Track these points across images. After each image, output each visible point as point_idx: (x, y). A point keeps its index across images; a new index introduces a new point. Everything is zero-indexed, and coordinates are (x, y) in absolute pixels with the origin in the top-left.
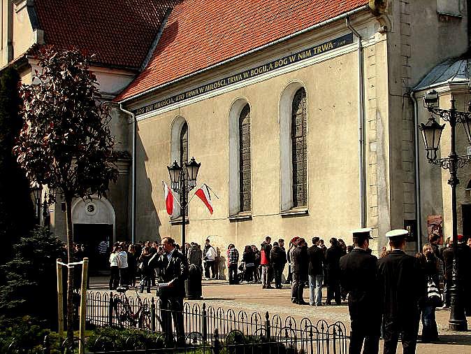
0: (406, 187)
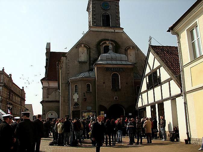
0: (66, 107)
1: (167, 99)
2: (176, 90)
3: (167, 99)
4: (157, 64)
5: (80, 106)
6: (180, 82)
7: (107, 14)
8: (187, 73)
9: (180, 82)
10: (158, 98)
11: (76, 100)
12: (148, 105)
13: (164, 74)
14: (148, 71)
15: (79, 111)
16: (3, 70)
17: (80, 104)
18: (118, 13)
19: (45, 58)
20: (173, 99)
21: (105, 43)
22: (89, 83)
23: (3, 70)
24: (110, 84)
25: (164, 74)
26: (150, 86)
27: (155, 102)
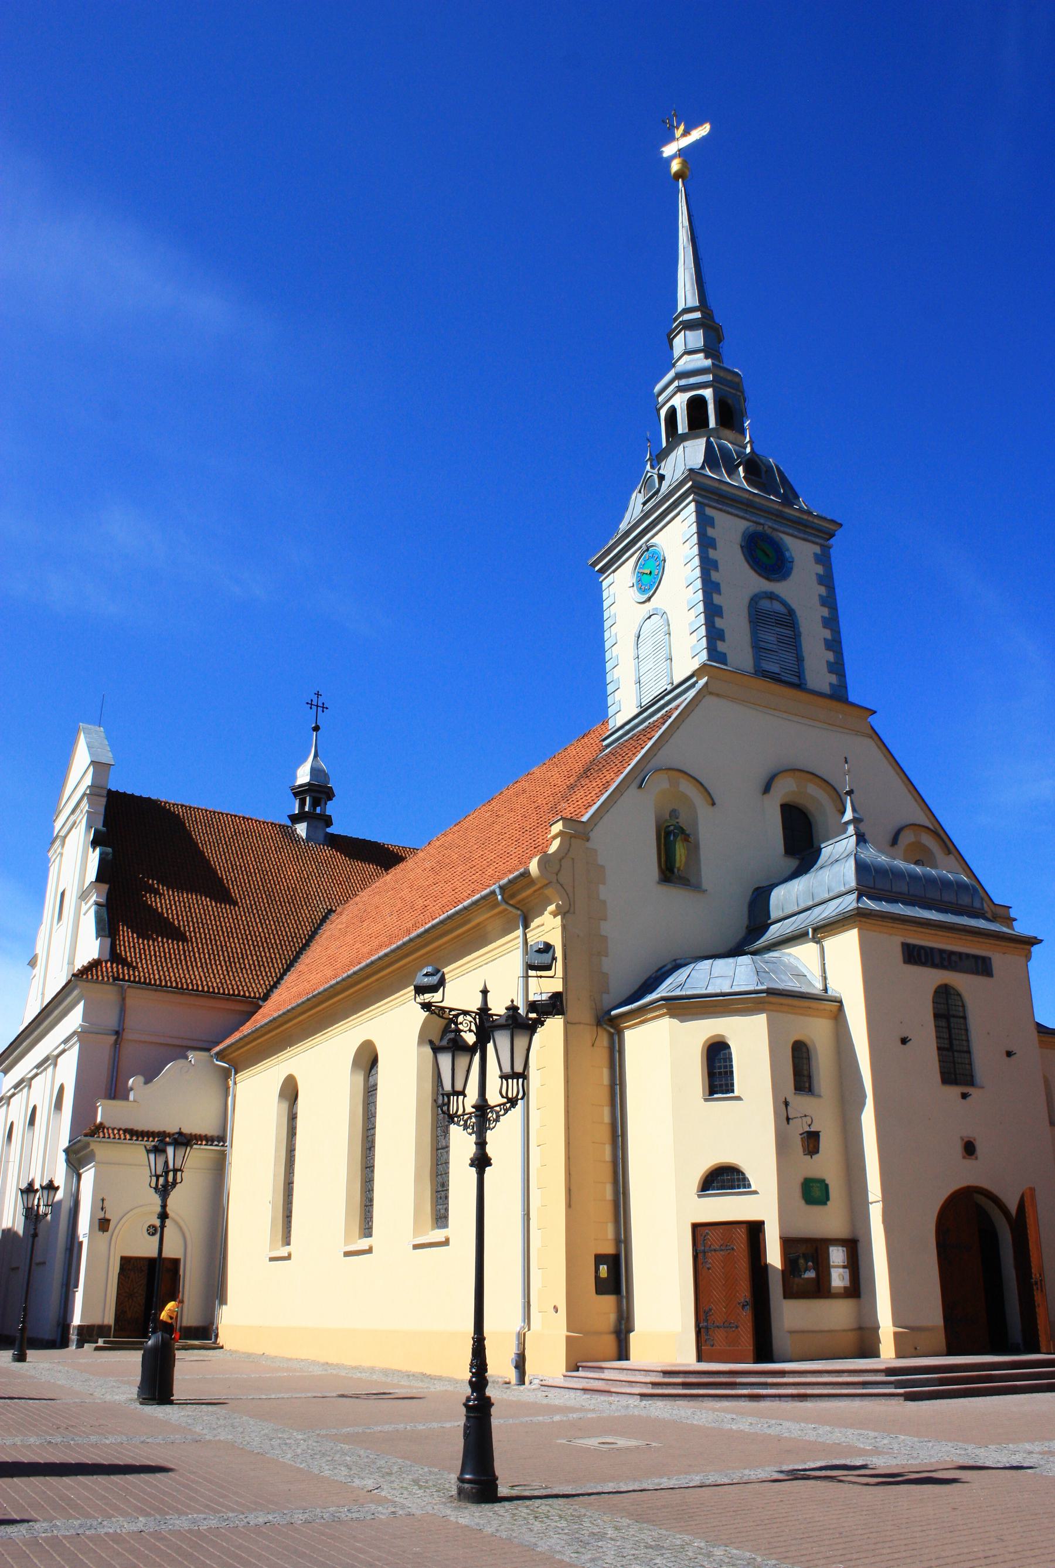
7: (777, 607)
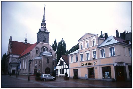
1: (65, 69)
2: (67, 67)
3: (65, 69)
4: (63, 60)
5: (37, 68)
6: (68, 66)
8: (70, 65)
9: (68, 66)
10: (62, 68)
11: (36, 66)
12: (59, 69)
13: (65, 63)
14: (60, 61)
15: (37, 69)
16: (26, 40)
17: (37, 67)
18: (48, 38)
19: (128, 67)
20: (66, 69)
21: (44, 47)
22: (40, 60)
23: (26, 40)
24: (46, 61)
25: (65, 63)
26: (60, 65)
27: (61, 69)
